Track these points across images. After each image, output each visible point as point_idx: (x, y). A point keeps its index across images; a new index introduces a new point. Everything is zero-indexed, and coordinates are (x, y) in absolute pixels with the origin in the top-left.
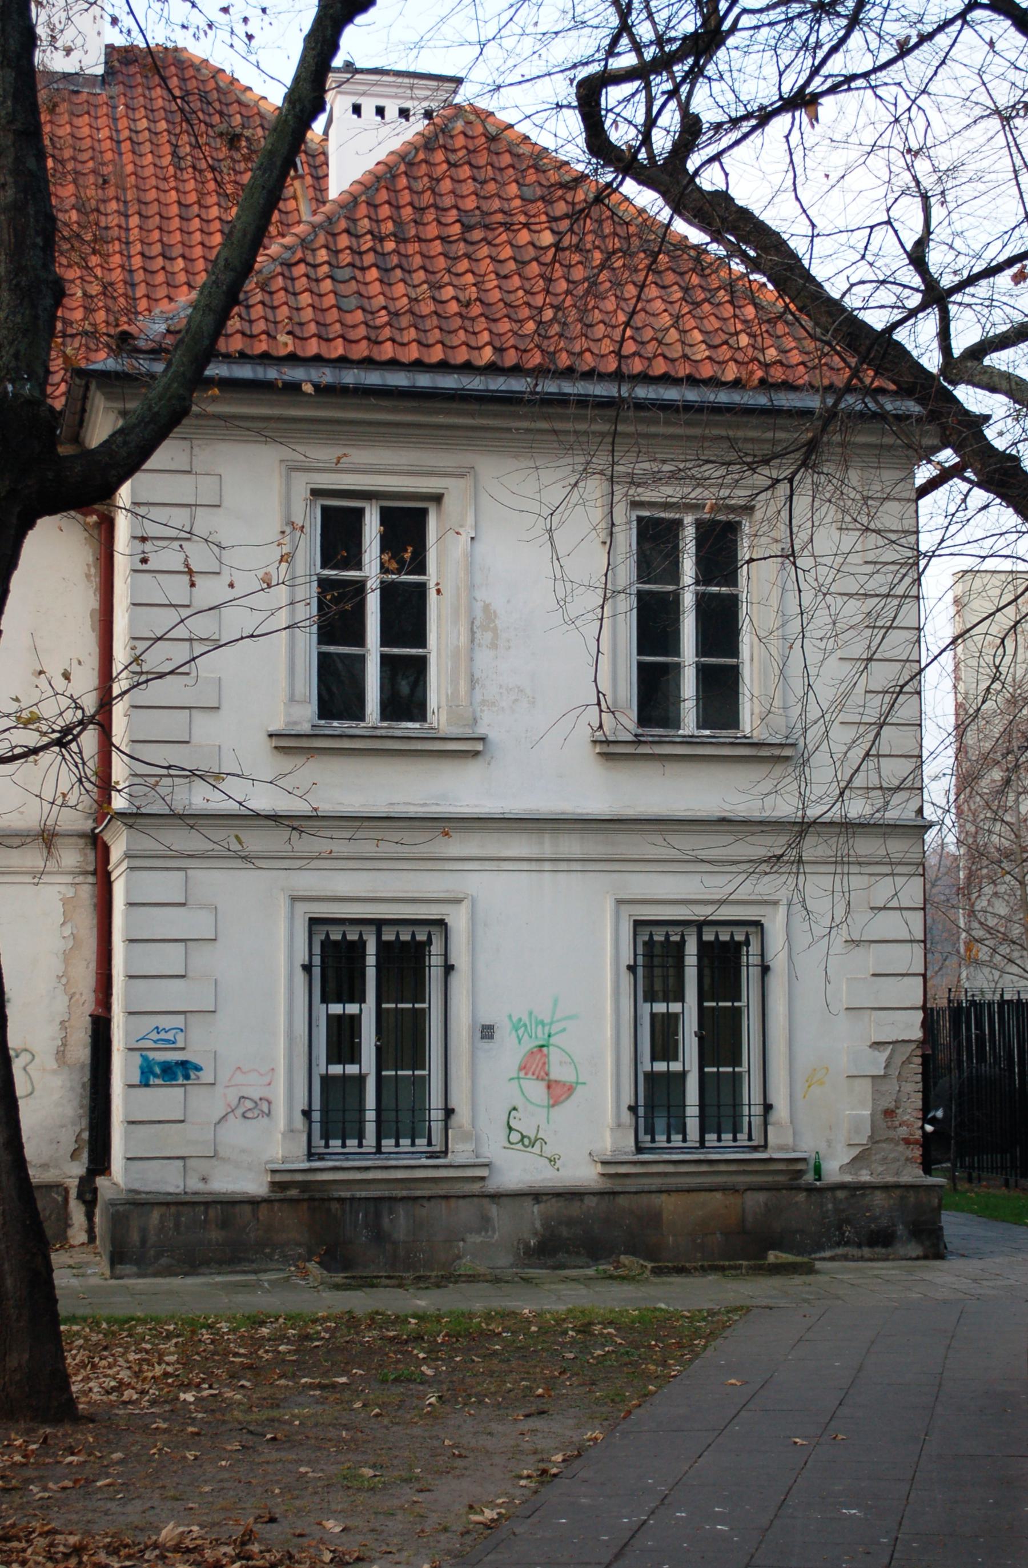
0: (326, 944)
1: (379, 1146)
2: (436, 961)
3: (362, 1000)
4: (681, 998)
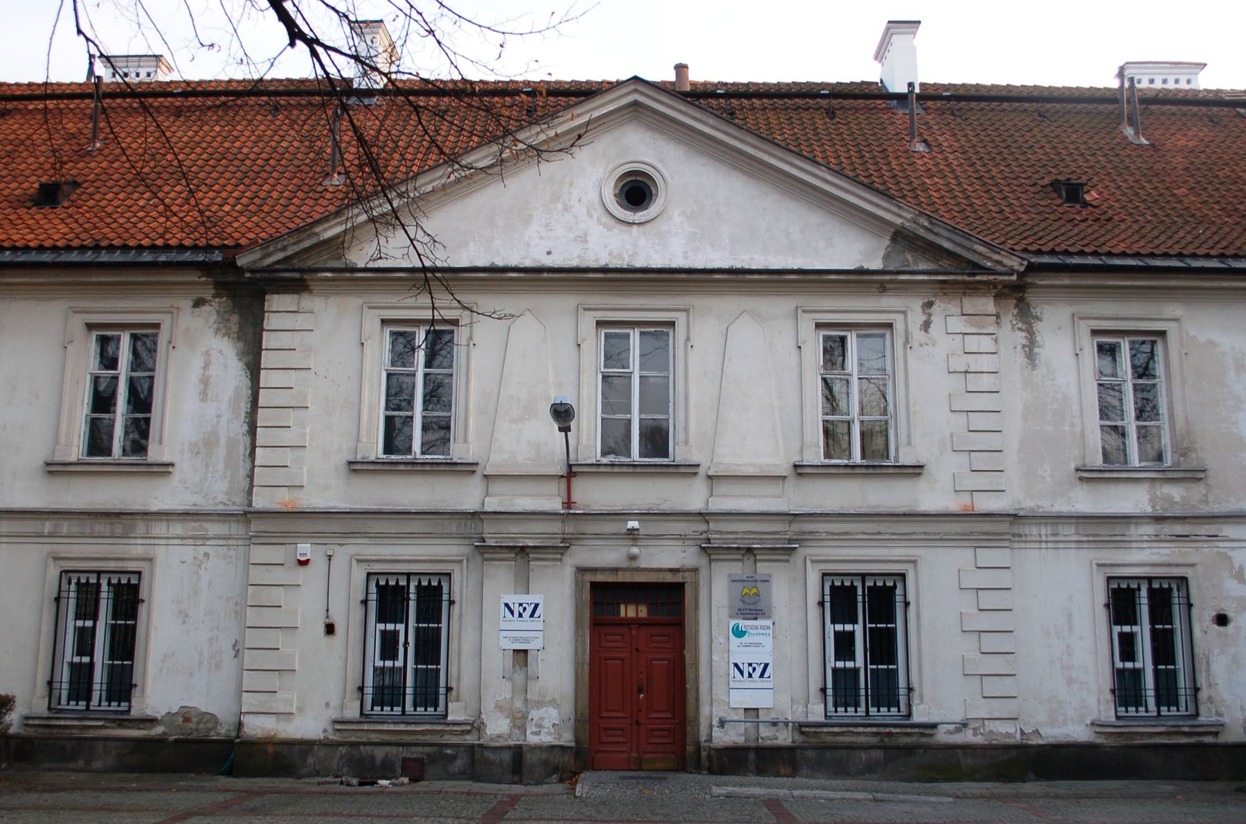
1: (1159, 711)
2: (899, 598)
3: (855, 622)
4: (95, 618)
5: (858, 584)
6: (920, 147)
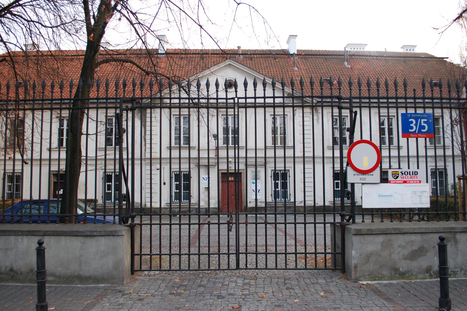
2: (288, 175)
5: (279, 172)
6: (296, 69)
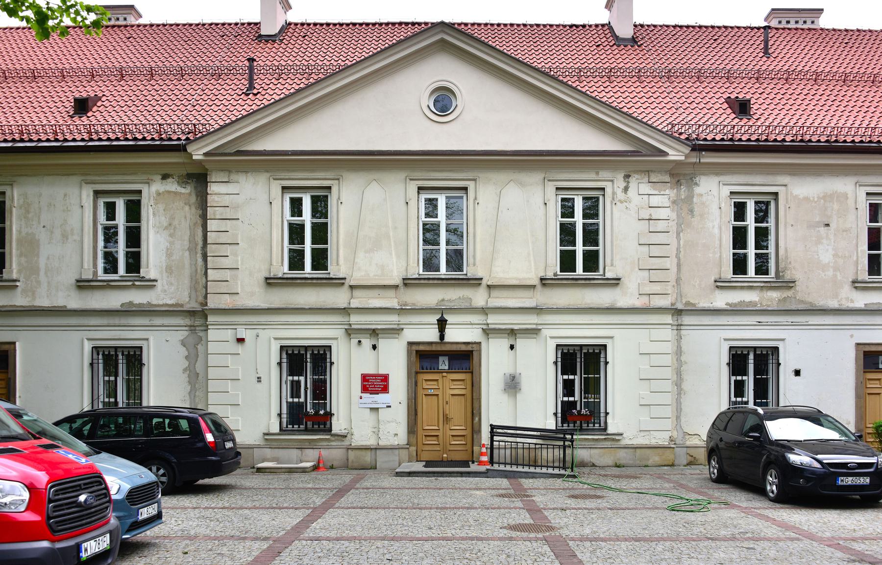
0: (562, 353)
1: (116, 352)
